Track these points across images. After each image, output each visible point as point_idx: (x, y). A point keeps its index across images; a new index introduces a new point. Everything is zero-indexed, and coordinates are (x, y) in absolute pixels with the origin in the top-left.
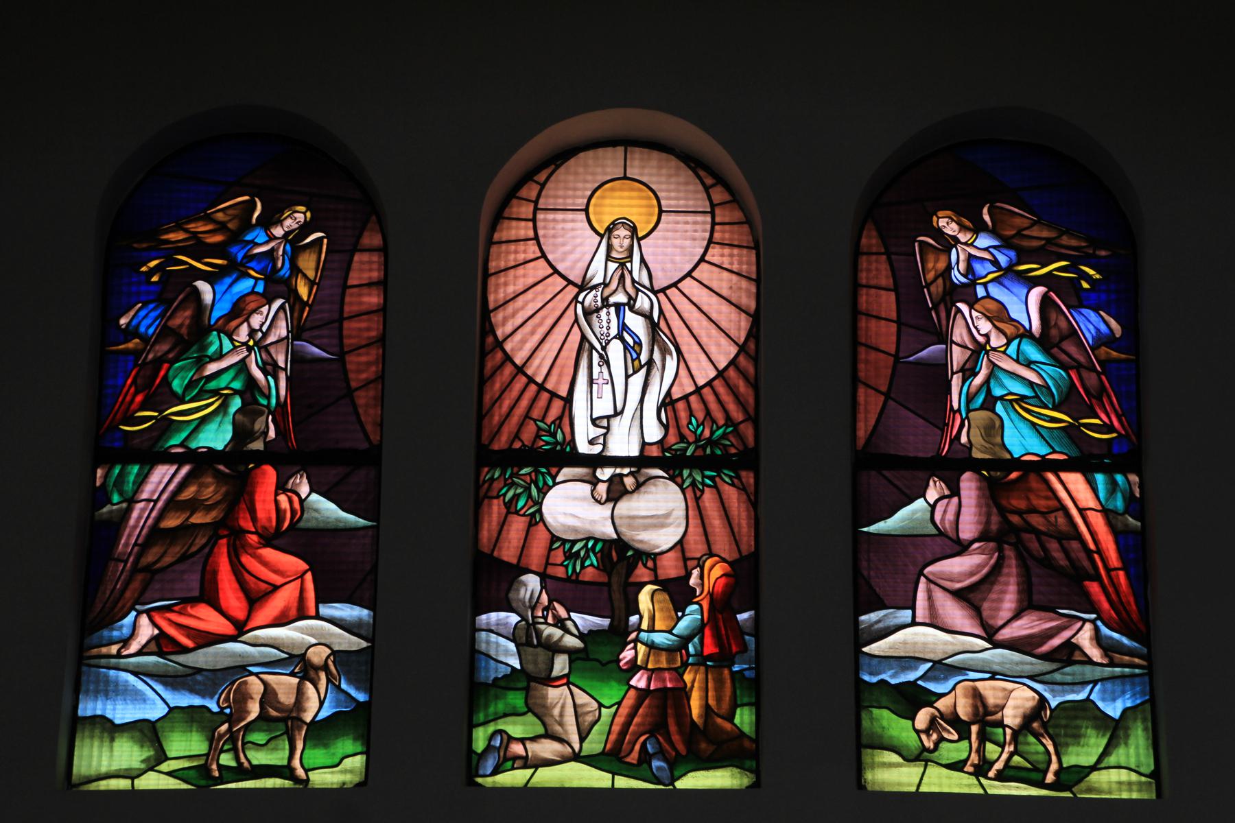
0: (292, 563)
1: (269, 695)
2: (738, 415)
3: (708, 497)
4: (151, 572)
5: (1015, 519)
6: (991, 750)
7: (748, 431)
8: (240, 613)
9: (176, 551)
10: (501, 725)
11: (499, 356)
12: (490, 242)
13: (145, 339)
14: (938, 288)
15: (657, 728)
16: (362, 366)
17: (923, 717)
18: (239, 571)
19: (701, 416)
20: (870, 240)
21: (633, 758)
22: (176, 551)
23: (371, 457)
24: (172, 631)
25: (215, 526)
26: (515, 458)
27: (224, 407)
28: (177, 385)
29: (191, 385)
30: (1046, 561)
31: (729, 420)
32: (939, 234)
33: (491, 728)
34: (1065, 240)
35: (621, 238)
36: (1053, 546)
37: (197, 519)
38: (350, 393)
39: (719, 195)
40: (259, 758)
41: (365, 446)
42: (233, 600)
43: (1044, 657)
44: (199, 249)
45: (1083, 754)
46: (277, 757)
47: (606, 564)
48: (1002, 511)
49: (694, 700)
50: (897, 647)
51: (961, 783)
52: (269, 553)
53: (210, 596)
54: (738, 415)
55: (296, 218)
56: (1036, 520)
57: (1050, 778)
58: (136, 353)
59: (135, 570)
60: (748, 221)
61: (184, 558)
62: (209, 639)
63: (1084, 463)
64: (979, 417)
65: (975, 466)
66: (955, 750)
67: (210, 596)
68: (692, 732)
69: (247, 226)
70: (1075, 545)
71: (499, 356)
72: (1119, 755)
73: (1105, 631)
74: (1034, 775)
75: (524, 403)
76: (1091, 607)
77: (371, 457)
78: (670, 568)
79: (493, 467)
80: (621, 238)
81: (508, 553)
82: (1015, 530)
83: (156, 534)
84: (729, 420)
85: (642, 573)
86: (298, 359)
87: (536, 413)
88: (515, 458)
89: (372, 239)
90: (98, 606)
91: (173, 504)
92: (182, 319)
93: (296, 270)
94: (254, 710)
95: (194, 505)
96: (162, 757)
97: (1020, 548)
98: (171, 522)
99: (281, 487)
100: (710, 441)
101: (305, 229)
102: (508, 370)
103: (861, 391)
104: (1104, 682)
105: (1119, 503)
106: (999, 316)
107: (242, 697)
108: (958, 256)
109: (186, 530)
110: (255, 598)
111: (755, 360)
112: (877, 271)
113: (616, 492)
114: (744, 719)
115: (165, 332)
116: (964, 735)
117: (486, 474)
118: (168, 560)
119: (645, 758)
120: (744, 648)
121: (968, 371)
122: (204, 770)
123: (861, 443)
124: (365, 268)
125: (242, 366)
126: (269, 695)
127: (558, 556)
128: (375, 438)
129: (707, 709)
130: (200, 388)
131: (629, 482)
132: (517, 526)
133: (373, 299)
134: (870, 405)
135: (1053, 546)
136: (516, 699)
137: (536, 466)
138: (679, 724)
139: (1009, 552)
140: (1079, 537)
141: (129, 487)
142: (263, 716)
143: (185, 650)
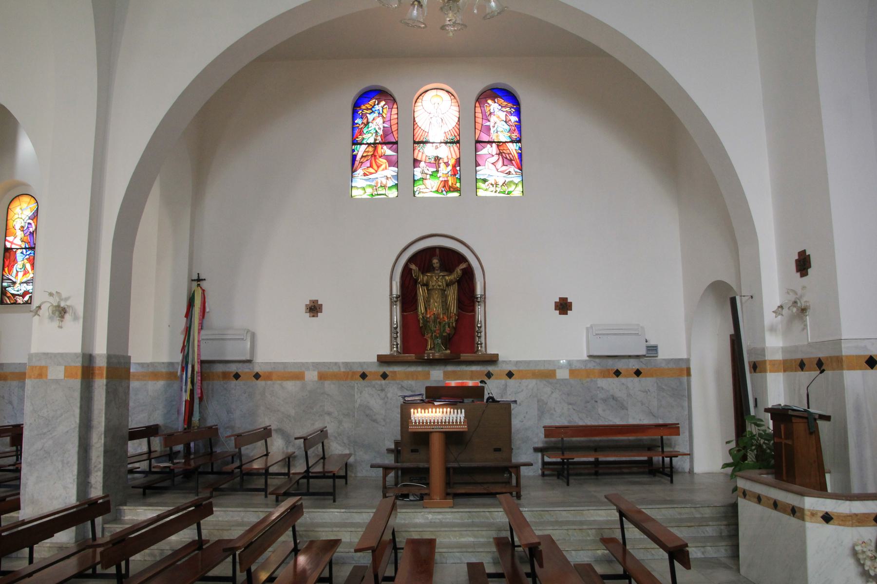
0: (385, 161)
1: (381, 183)
2: (456, 135)
3: (452, 149)
4: (362, 163)
5: (501, 151)
6: (497, 189)
7: (458, 137)
8: (376, 169)
9: (366, 159)
10: (419, 186)
11: (417, 125)
12: (415, 106)
13: (359, 125)
14: (488, 113)
15: (444, 186)
16: (394, 128)
17: (487, 183)
18: (376, 162)
19: (450, 134)
20: (477, 105)
21: (440, 192)
22: (366, 159)
23: (396, 143)
24: (366, 172)
25: (372, 155)
26: (419, 143)
27: (372, 135)
28: (365, 132)
29: (367, 132)
30: (506, 158)
31: (455, 136)
32: (488, 104)
33: (417, 187)
34: (509, 105)
35: (436, 105)
36: (507, 155)
37: (369, 154)
38: (392, 132)
39: (452, 97)
40: (379, 192)
41: (395, 141)
42: (375, 167)
43: (506, 174)
44: (367, 109)
45: (510, 189)
46: (384, 192)
47: (435, 160)
48: (499, 150)
49: (291, 541)
50: (73, 314)
51: (493, 194)
52: (380, 159)
53: (371, 166)
54: (456, 135)
55: (383, 103)
56: (504, 151)
57: (506, 193)
58: (358, 127)
59: (360, 162)
60: (457, 102)
61: (367, 160)
62: (371, 173)
63: (512, 142)
64: (496, 134)
65: (495, 142)
66: (493, 189)
67: (371, 166)
68: (450, 188)
69: (375, 105)
70: (510, 155)
71: (417, 125)
72: (517, 189)
73: (515, 169)
74: (504, 192)
75: (421, 133)
76: (514, 165)
77: (396, 143)
78: (446, 160)
79: (416, 144)
80: (436, 105)
81: (419, 158)
82: (500, 153)
83: (363, 156)
84: (455, 136)
85: (441, 161)
86: (384, 127)
87: (423, 135)
88: (419, 143)
89: (395, 106)
90: (354, 168)
91: (365, 152)
92: (365, 121)
93: (383, 112)
94: (379, 185)
95: (368, 152)
96: (365, 192)
97: (502, 155)
98: (365, 155)
99: (382, 148)
100: (452, 139)
101: (384, 105)
102: (418, 128)
103: (476, 130)
104: (7, 235)
105: (518, 148)
106: (498, 117)
107: (377, 183)
108: (492, 108)
109: (367, 156)
110: (378, 167)
111: (459, 125)
112: (478, 110)
113: (437, 148)
114: (458, 185)
115: (363, 123)
116: (493, 186)
117: (415, 145)
118: (365, 161)
119: (442, 191)
120: (458, 173)
121: (494, 127)
122: (372, 194)
123: (476, 139)
124: (394, 111)
125: (375, 129)
126: (381, 183)
127: (427, 159)
128: (397, 140)
129: (452, 183)
130: (368, 132)
131: (439, 146)
132: (420, 154)
133: (396, 116)
134: (478, 132)
135: (507, 155)
136: (421, 182)
137: (423, 144)
138: (448, 186)
139: (500, 156)
140: (511, 154)
141: (358, 149)
142: (381, 186)
143: (368, 175)
